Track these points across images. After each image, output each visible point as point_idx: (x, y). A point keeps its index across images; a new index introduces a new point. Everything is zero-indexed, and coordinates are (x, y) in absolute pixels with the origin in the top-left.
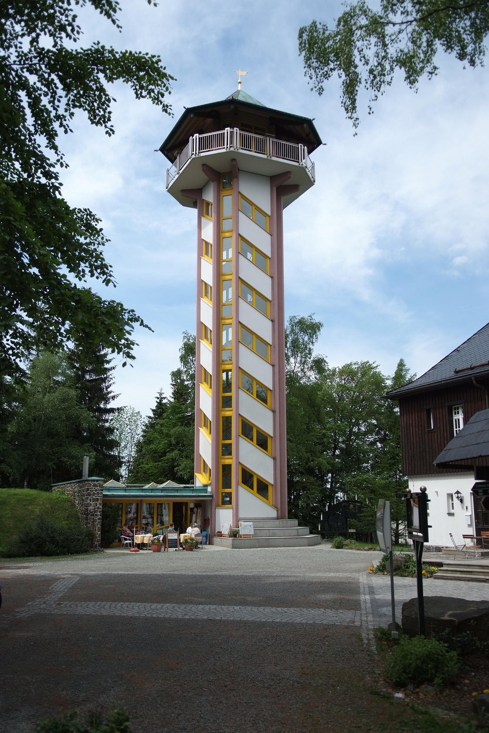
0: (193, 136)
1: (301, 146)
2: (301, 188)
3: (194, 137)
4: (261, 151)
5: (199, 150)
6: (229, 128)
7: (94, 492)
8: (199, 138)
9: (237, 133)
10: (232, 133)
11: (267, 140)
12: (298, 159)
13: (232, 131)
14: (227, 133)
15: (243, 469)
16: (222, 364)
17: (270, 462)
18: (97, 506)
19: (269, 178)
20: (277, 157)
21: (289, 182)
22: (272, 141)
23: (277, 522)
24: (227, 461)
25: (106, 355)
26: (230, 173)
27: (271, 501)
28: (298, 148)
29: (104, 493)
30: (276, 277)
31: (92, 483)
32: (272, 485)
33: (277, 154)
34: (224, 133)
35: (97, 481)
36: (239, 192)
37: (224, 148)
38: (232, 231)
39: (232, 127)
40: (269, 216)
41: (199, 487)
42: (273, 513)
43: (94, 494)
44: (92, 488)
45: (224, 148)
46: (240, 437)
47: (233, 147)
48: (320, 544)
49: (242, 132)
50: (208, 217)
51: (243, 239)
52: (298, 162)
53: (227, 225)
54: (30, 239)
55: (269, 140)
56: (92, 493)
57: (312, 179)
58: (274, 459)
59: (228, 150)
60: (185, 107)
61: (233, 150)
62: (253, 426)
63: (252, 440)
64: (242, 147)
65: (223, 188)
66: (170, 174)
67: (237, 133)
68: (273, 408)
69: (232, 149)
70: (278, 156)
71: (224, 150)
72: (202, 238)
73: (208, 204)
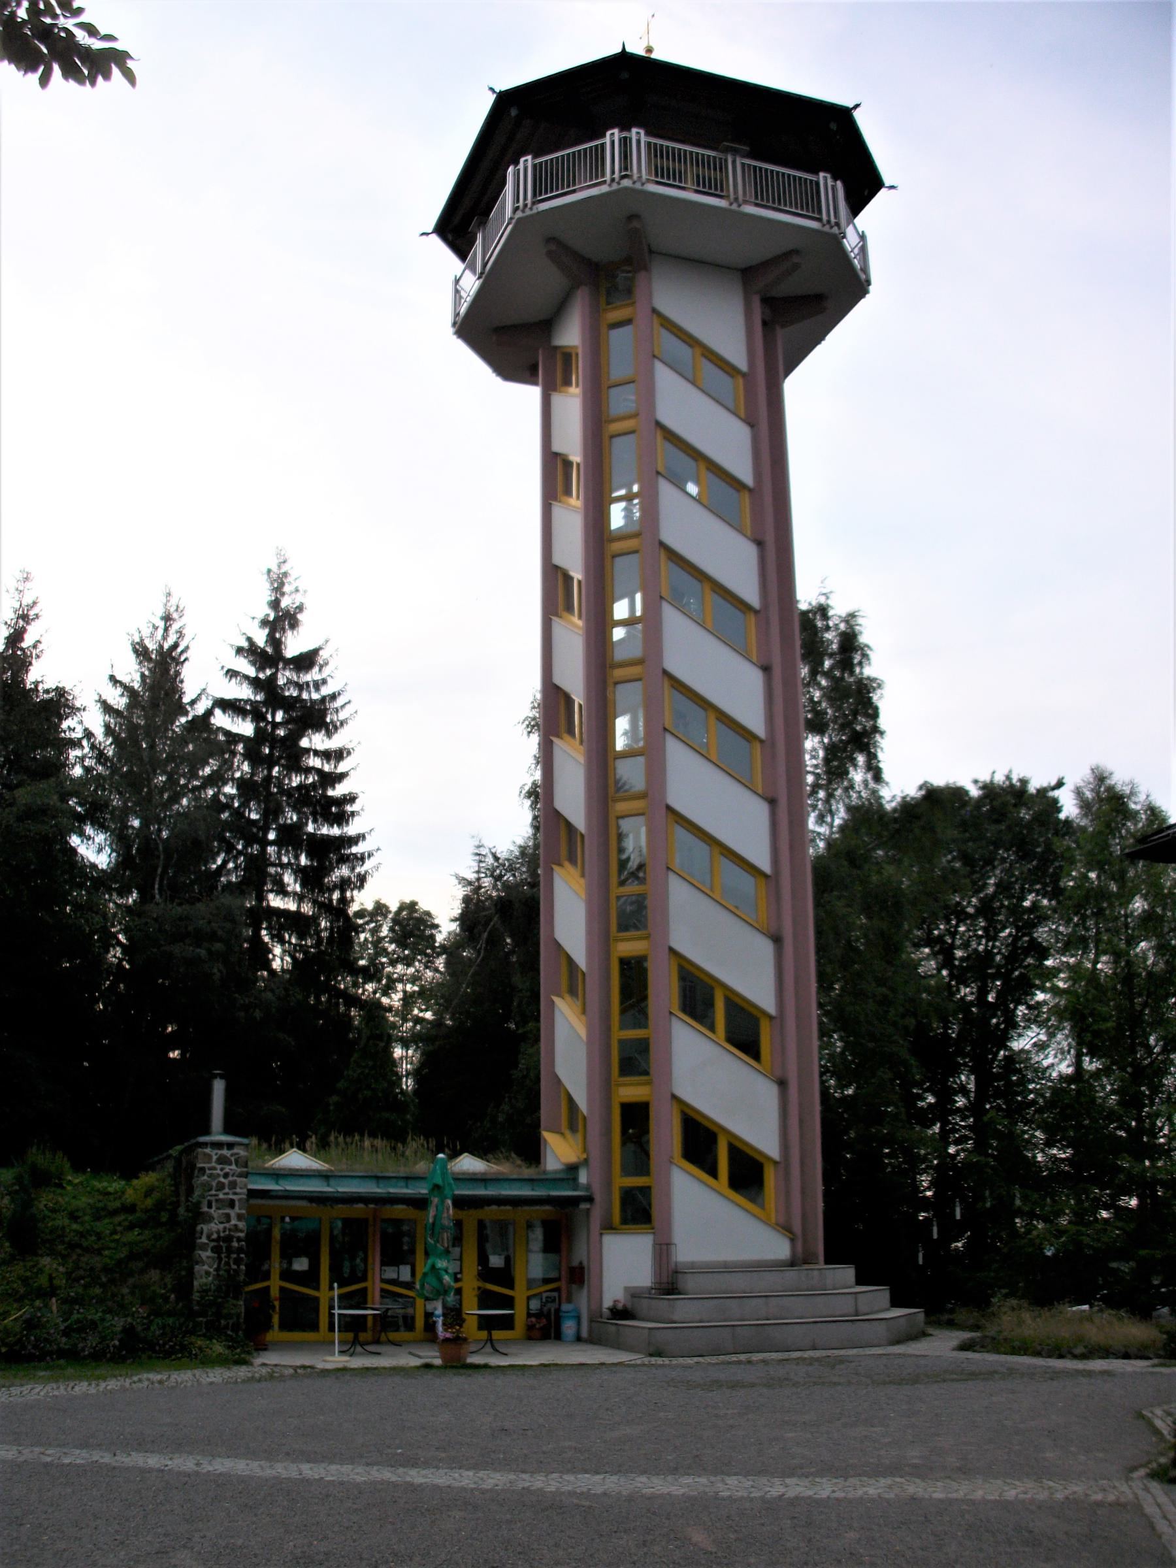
0: (516, 163)
1: (825, 178)
3: (521, 166)
4: (710, 188)
5: (534, 195)
6: (616, 131)
7: (222, 1180)
8: (534, 166)
9: (639, 142)
10: (625, 142)
11: (726, 161)
12: (820, 212)
13: (625, 138)
14: (613, 143)
15: (681, 969)
16: (615, 801)
17: (768, 1093)
18: (229, 1220)
20: (757, 205)
22: (743, 165)
23: (791, 1275)
25: (338, 921)
26: (628, 261)
27: (773, 1210)
28: (817, 184)
29: (251, 1187)
30: (770, 539)
31: (214, 1154)
32: (776, 1163)
33: (756, 197)
34: (603, 145)
35: (230, 1146)
36: (654, 311)
37: (605, 182)
38: (635, 415)
39: (626, 127)
40: (744, 375)
41: (556, 1172)
42: (780, 1249)
43: (221, 1187)
44: (214, 1169)
45: (605, 182)
46: (674, 1020)
48: (924, 1334)
49: (653, 140)
51: (678, 685)
52: (819, 220)
53: (621, 401)
54: (410, 1137)
55: (734, 162)
56: (214, 1184)
57: (863, 276)
58: (782, 1083)
59: (615, 186)
60: (492, 89)
62: (713, 984)
63: (713, 1172)
65: (608, 303)
67: (639, 142)
69: (626, 183)
70: (759, 202)
71: (604, 189)
73: (567, 357)
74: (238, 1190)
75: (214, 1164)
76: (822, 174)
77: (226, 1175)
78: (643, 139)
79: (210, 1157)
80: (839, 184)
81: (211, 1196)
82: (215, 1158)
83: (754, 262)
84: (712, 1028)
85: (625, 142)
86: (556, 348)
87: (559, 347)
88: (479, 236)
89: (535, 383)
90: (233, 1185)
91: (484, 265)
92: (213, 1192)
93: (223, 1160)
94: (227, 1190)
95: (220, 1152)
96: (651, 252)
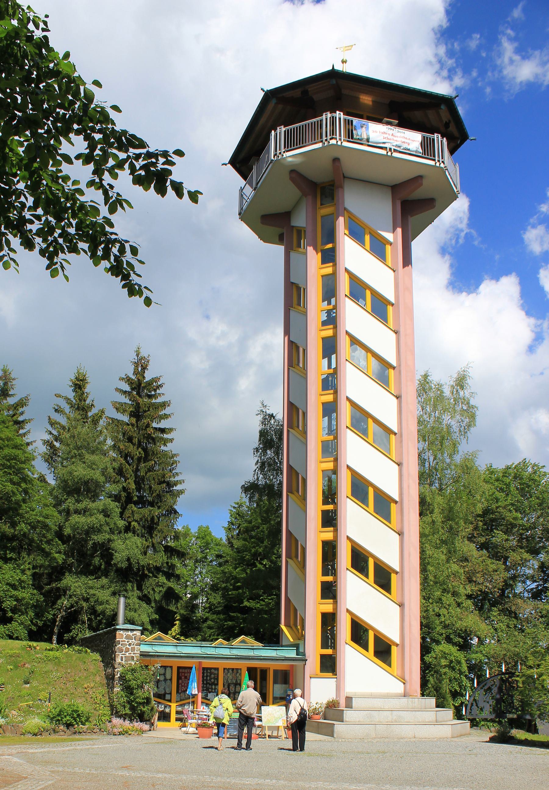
0: (275, 130)
2: (438, 204)
7: (128, 646)
9: (340, 119)
12: (434, 156)
14: (326, 119)
19: (390, 188)
21: (419, 193)
23: (404, 700)
24: (328, 270)
28: (433, 140)
34: (321, 121)
35: (132, 630)
42: (399, 687)
44: (125, 641)
47: (336, 139)
50: (299, 308)
52: (434, 160)
56: (124, 649)
61: (335, 143)
63: (366, 648)
64: (349, 138)
65: (321, 204)
66: (244, 196)
67: (340, 119)
68: (399, 600)
72: (292, 280)
74: (136, 652)
75: (124, 639)
76: (436, 134)
77: (130, 645)
78: (342, 116)
79: (122, 635)
80: (445, 139)
81: (122, 654)
82: (125, 636)
83: (397, 183)
84: (367, 576)
85: (333, 119)
86: (293, 227)
87: (295, 227)
88: (255, 167)
89: (283, 245)
90: (133, 649)
91: (257, 184)
92: (124, 653)
93: (128, 637)
94: (130, 652)
95: (127, 633)
96: (344, 177)
